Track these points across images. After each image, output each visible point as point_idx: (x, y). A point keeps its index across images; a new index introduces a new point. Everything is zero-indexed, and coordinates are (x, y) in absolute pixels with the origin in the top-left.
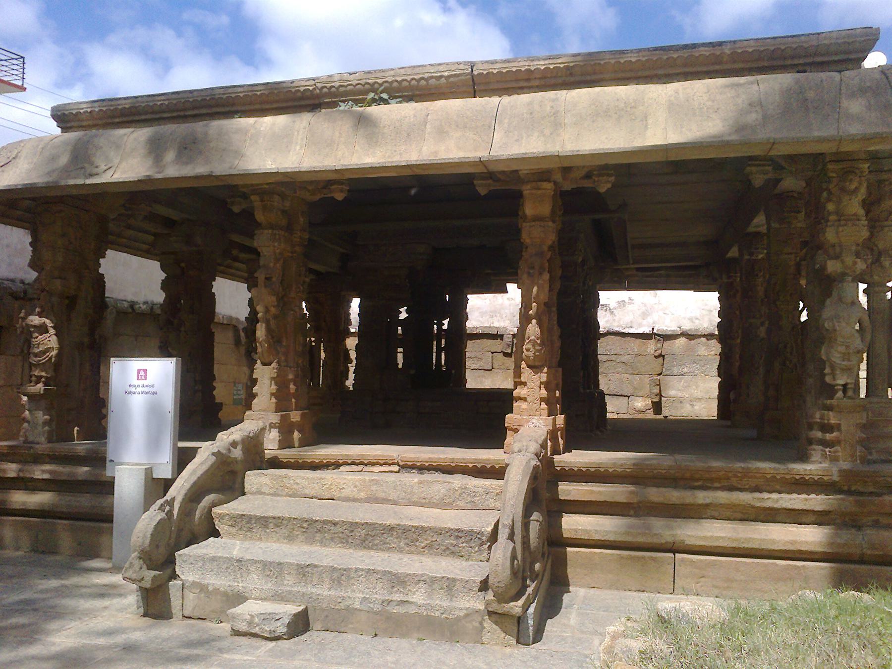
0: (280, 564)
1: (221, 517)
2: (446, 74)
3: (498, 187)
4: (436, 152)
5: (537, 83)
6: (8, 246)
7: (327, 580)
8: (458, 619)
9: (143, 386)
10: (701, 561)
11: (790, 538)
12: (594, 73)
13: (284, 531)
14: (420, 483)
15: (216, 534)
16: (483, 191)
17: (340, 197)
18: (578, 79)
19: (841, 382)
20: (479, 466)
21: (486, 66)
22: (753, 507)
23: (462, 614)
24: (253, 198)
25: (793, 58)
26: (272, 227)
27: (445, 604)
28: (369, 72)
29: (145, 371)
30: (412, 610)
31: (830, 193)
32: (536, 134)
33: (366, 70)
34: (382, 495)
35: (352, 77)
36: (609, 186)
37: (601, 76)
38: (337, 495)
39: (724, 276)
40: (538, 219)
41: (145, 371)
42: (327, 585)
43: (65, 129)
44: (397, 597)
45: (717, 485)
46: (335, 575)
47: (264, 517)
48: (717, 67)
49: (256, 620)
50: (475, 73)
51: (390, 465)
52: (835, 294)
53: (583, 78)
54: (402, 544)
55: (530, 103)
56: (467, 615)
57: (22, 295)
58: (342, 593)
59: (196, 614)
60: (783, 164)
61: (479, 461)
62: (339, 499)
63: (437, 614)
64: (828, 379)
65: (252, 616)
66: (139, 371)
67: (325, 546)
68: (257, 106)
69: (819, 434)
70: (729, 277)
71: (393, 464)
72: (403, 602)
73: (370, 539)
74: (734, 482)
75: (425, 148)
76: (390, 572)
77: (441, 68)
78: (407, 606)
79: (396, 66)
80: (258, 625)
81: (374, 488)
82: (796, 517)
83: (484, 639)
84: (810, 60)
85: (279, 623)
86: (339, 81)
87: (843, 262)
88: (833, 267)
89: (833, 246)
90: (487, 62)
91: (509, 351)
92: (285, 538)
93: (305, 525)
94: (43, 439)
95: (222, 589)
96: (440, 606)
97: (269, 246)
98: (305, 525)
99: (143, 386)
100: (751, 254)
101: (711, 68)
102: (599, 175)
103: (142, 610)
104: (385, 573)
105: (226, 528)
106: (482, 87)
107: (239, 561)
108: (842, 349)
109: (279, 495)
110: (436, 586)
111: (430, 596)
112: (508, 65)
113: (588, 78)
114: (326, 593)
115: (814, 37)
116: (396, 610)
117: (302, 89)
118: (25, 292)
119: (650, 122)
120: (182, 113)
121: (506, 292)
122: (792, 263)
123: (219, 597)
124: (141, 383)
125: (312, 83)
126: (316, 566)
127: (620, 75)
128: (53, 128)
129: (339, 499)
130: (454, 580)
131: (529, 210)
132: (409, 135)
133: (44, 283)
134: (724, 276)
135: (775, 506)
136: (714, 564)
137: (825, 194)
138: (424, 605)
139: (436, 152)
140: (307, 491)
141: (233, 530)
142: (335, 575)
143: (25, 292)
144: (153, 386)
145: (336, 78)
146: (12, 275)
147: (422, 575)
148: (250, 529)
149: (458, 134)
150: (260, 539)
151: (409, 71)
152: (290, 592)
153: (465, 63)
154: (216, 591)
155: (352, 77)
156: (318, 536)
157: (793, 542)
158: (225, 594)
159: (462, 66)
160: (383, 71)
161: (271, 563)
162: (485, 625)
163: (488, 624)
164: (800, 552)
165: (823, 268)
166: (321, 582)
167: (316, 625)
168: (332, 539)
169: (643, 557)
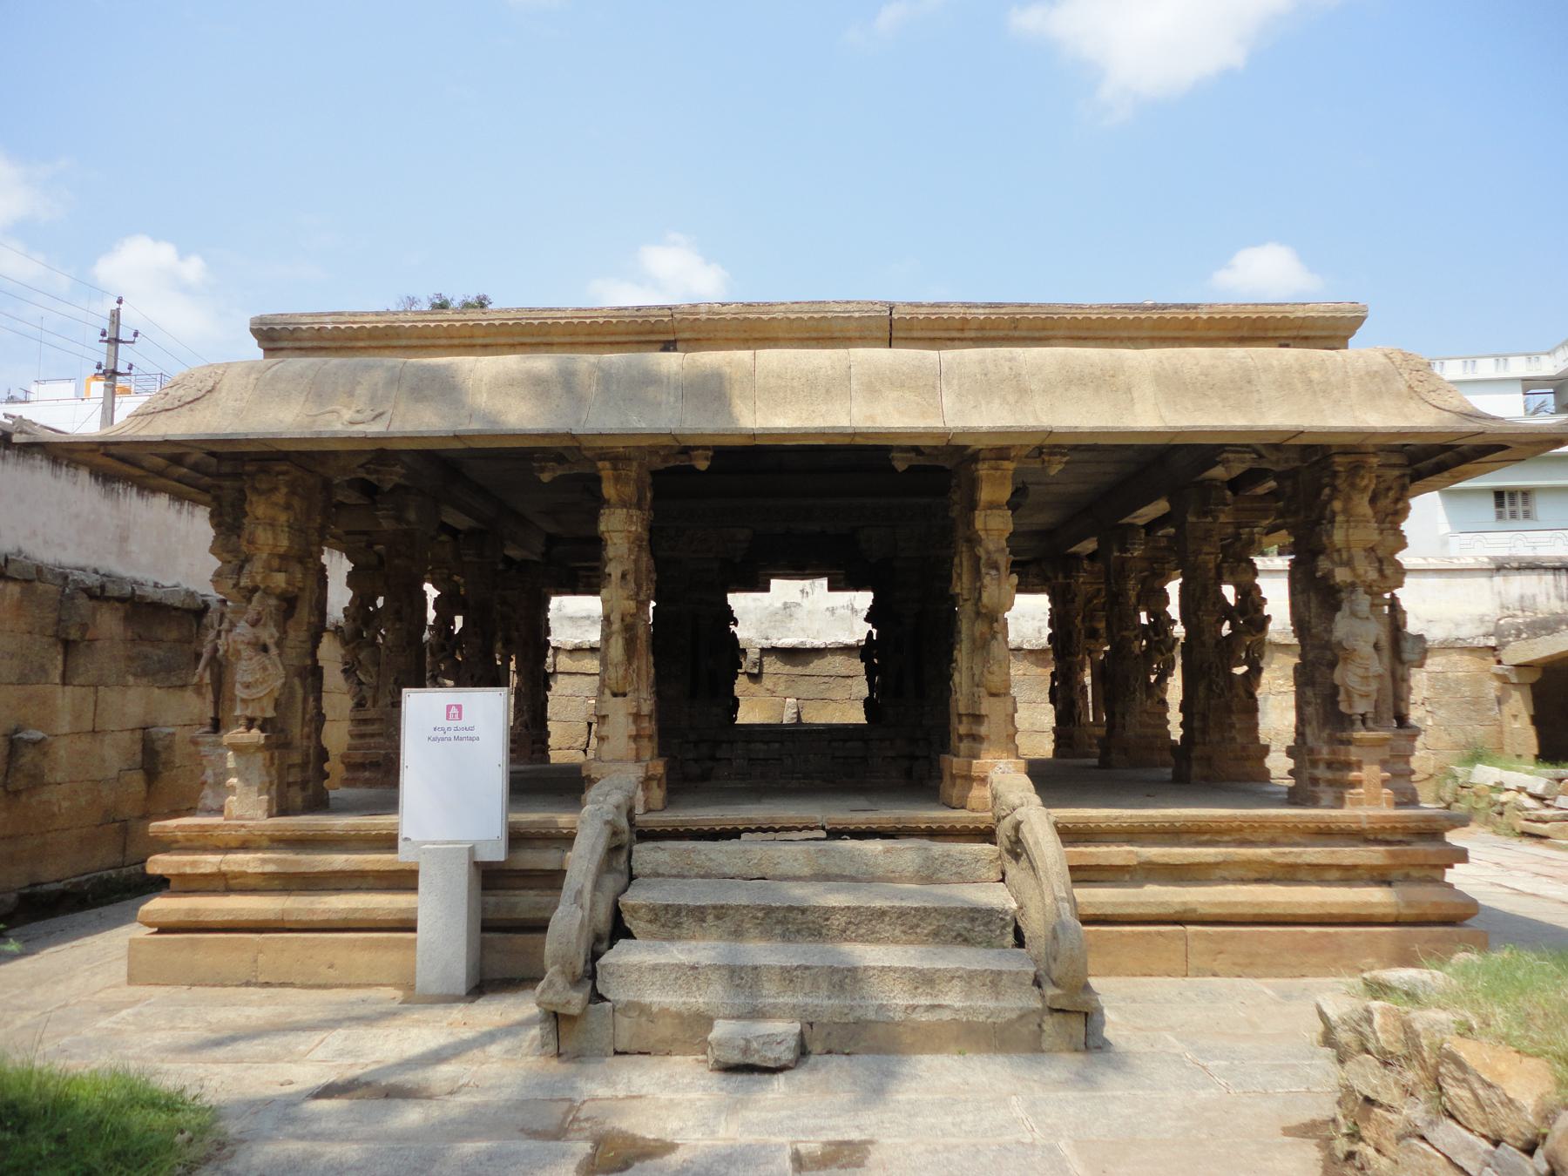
0: (755, 968)
1: (634, 910)
2: (857, 315)
3: (921, 461)
4: (872, 418)
5: (972, 334)
6: (77, 516)
7: (824, 985)
8: (1010, 1023)
9: (456, 729)
10: (1218, 933)
11: (1319, 899)
12: (1044, 329)
13: (729, 924)
14: (887, 851)
15: (629, 935)
16: (900, 466)
17: (703, 465)
18: (1024, 334)
19: (1361, 711)
20: (934, 826)
21: (908, 309)
22: (1272, 863)
23: (1014, 1016)
24: (600, 464)
25: (1276, 329)
26: (624, 504)
27: (991, 1004)
28: (749, 305)
29: (459, 707)
30: (946, 1016)
31: (1335, 489)
32: (997, 401)
33: (746, 301)
34: (836, 870)
35: (725, 309)
36: (1060, 467)
37: (1050, 333)
38: (770, 872)
39: (1060, 576)
40: (992, 506)
41: (459, 707)
42: (824, 992)
43: (269, 351)
44: (924, 1001)
45: (1226, 838)
46: (836, 978)
47: (699, 907)
48: (1189, 334)
49: (755, 1045)
50: (895, 316)
51: (812, 829)
52: (1345, 607)
53: (1030, 334)
54: (897, 932)
55: (982, 361)
56: (1021, 1017)
57: (98, 591)
58: (848, 1002)
59: (635, 1047)
60: (1264, 452)
61: (934, 820)
62: (774, 878)
63: (981, 1018)
64: (1343, 707)
65: (748, 1041)
66: (449, 708)
67: (789, 940)
68: (583, 339)
69: (1329, 775)
70: (1066, 577)
71: (816, 828)
72: (933, 1007)
73: (853, 928)
74: (1247, 835)
75: (854, 410)
76: (912, 969)
77: (849, 307)
78: (938, 1011)
79: (788, 299)
80: (758, 1051)
81: (823, 861)
82: (1349, 875)
83: (1045, 1046)
84: (1295, 333)
85: (783, 1048)
86: (708, 313)
87: (1353, 569)
88: (1341, 575)
89: (1339, 551)
90: (910, 304)
91: (756, 671)
92: (730, 934)
93: (760, 915)
94: (260, 812)
95: (673, 1009)
96: (985, 1008)
97: (620, 530)
98: (760, 915)
99: (456, 729)
100: (1124, 550)
101: (1184, 334)
102: (1052, 454)
103: (552, 1048)
104: (905, 970)
105: (642, 924)
106: (901, 334)
107: (693, 968)
108: (1360, 672)
109: (684, 877)
110: (976, 982)
111: (968, 996)
112: (936, 310)
113: (1037, 334)
114: (826, 1002)
115: (1301, 308)
116: (925, 1017)
117: (653, 320)
118: (103, 587)
119: (1135, 395)
120: (467, 341)
121: (767, 589)
122: (1211, 565)
123: (668, 1020)
124: (452, 724)
125: (668, 312)
126: (807, 968)
127: (1076, 334)
128: (252, 351)
129: (774, 878)
130: (1000, 973)
131: (985, 495)
132: (828, 391)
133: (259, 578)
134: (1060, 576)
135: (1299, 861)
136: (1232, 936)
137: (1327, 491)
138: (963, 1008)
139: (872, 418)
140: (726, 870)
141: (654, 928)
142: (836, 978)
143: (103, 587)
144: (472, 729)
145: (703, 309)
146: (82, 562)
147: (957, 969)
148: (678, 925)
149: (895, 394)
150: (693, 937)
151: (806, 308)
152: (775, 1006)
153: (882, 303)
154: (664, 1012)
155: (725, 309)
156: (778, 930)
157: (1322, 904)
158: (679, 1015)
159: (877, 307)
160: (771, 305)
161: (742, 968)
162: (1045, 1027)
163: (1050, 1023)
164: (1331, 915)
165: (1329, 575)
166: (815, 986)
167: (816, 1047)
168: (798, 931)
169: (1149, 933)
